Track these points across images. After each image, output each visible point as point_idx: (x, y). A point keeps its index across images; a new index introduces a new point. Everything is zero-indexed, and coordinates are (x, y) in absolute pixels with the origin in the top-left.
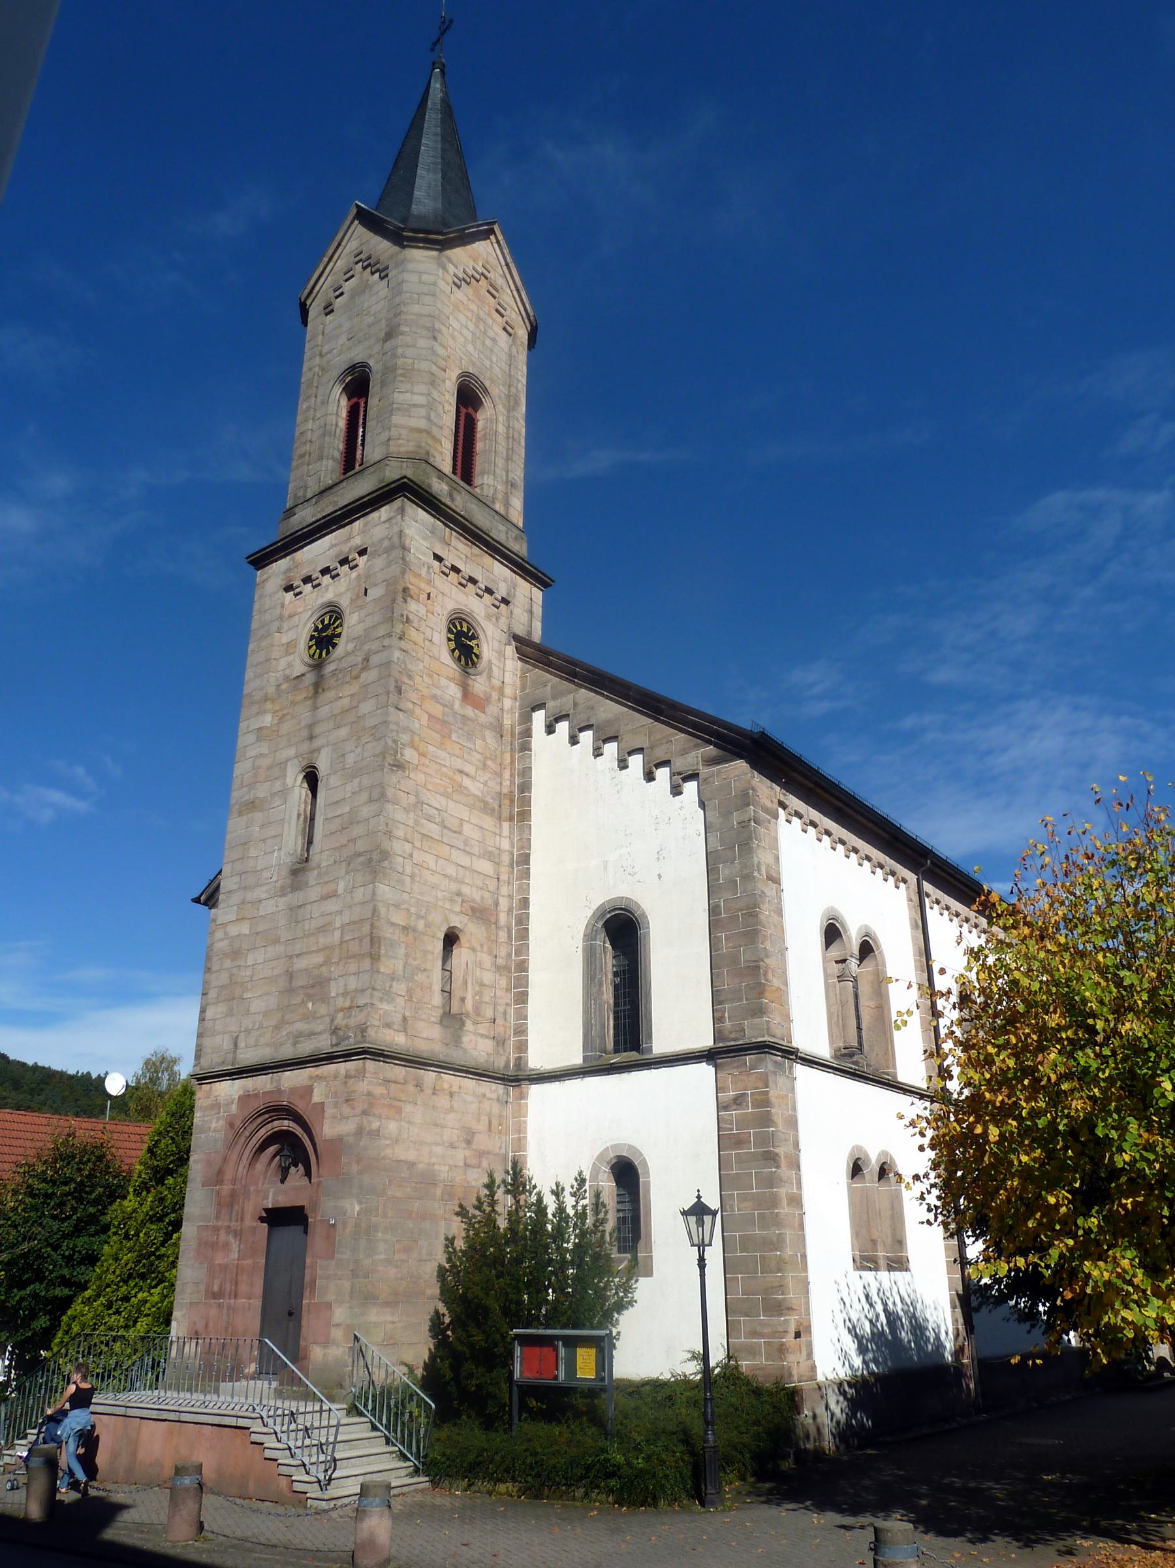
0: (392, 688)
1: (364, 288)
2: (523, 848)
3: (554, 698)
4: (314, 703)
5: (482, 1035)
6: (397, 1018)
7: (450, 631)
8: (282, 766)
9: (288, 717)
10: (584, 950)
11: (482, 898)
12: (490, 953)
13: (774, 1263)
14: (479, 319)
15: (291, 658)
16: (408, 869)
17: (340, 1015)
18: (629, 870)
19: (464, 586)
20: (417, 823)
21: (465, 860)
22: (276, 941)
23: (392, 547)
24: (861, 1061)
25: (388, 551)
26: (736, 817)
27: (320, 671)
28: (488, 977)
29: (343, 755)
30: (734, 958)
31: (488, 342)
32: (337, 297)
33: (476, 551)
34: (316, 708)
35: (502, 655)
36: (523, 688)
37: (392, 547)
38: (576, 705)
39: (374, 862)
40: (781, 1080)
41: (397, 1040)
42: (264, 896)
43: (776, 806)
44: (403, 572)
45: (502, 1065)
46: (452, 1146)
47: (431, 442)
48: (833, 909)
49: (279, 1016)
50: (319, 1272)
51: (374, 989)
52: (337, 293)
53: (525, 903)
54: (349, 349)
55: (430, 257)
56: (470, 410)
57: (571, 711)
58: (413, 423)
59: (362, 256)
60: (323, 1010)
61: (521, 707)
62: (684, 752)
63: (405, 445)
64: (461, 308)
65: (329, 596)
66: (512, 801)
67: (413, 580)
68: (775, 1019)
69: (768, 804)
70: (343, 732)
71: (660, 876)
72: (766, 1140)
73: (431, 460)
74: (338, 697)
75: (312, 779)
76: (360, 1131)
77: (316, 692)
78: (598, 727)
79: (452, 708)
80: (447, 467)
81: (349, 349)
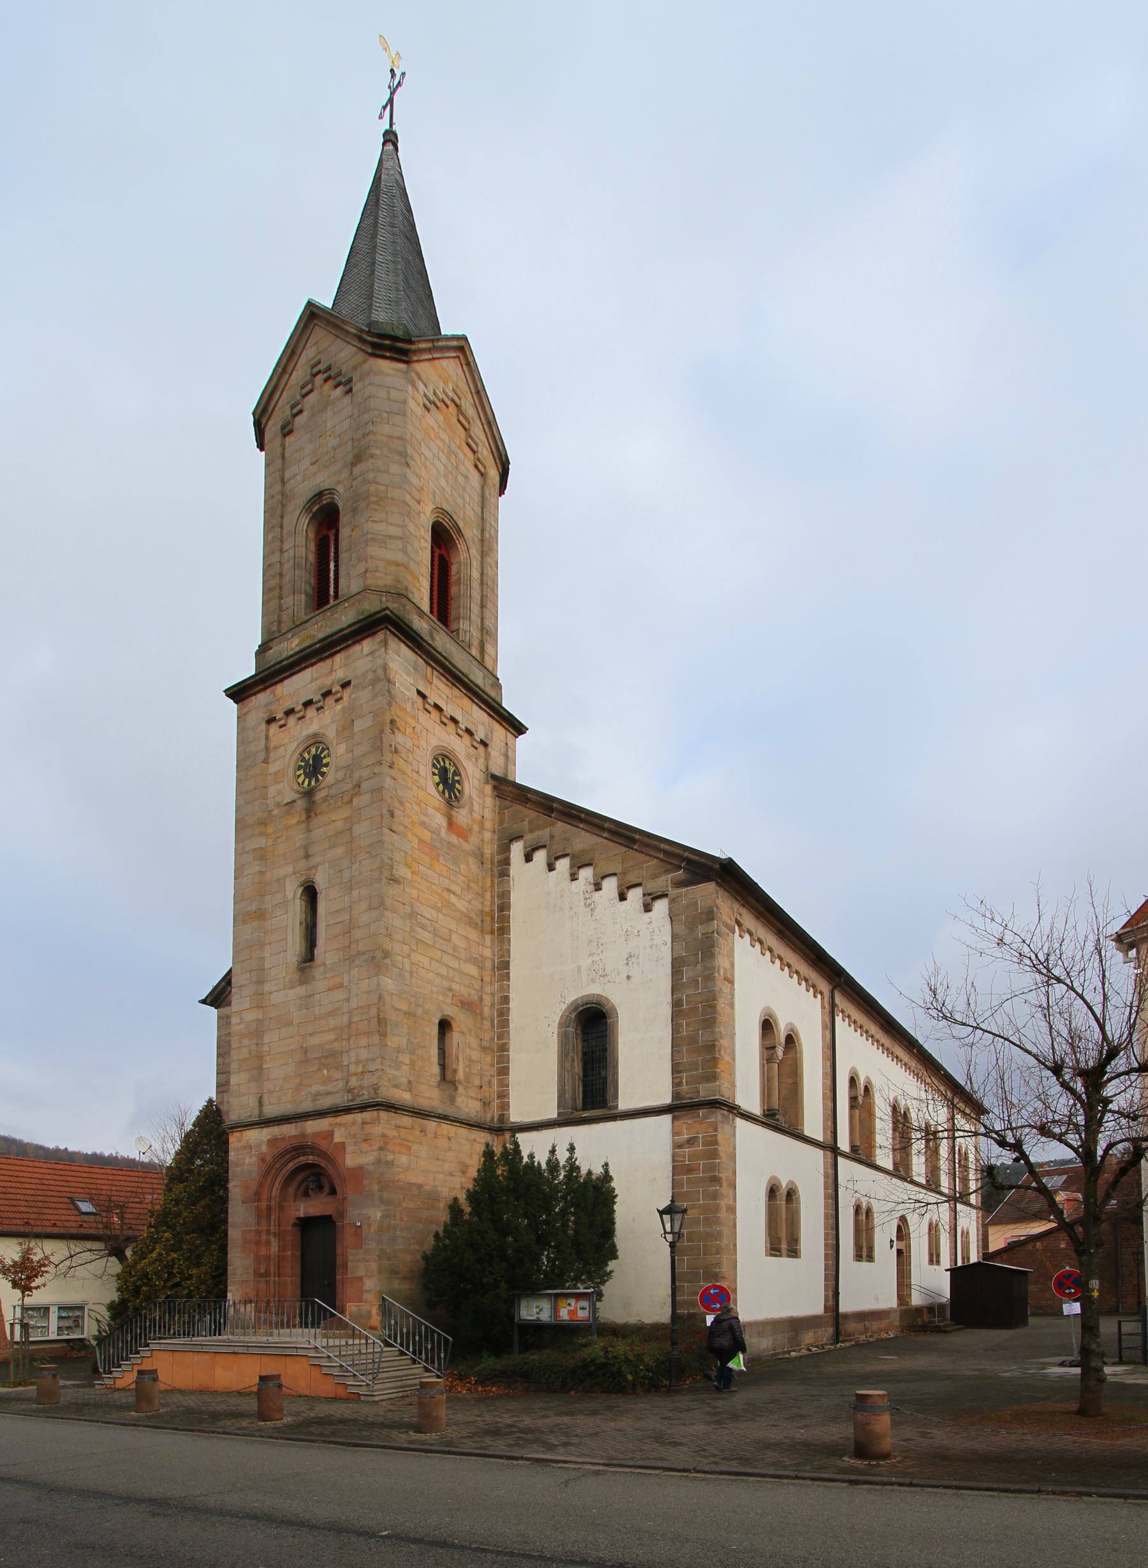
0: (385, 812)
1: (325, 405)
2: (502, 956)
3: (531, 831)
4: (308, 826)
5: (471, 1098)
6: (404, 1081)
7: (434, 766)
8: (281, 881)
9: (282, 839)
11: (469, 994)
12: (477, 1036)
13: (714, 1250)
14: (450, 451)
15: (280, 786)
16: (407, 967)
17: (354, 1079)
18: (601, 972)
19: (445, 724)
20: (412, 930)
21: (454, 964)
22: (291, 1024)
23: (377, 680)
24: (781, 1117)
25: (373, 683)
26: (701, 930)
27: (310, 798)
28: (475, 1055)
29: (341, 871)
30: (693, 1040)
31: (461, 479)
32: (295, 416)
33: (456, 692)
34: (309, 831)
35: (481, 792)
36: (501, 822)
37: (377, 680)
38: (552, 837)
39: (377, 960)
40: (727, 1128)
41: (406, 1097)
42: (273, 989)
43: (733, 923)
44: (390, 705)
45: (488, 1119)
46: (451, 1174)
47: (409, 578)
48: (768, 1008)
49: (297, 1080)
50: (350, 1258)
51: (383, 1058)
52: (295, 411)
53: (506, 1000)
54: (315, 474)
55: (398, 370)
56: (443, 552)
58: (390, 555)
59: (321, 367)
60: (338, 1075)
61: (500, 839)
62: (655, 876)
63: (383, 580)
64: (432, 435)
65: (314, 728)
66: (493, 918)
67: (399, 713)
68: (724, 1085)
69: (729, 921)
70: (340, 851)
72: (712, 1168)
73: (410, 596)
74: (331, 821)
75: (311, 894)
76: (378, 1161)
77: (308, 817)
79: (439, 835)
80: (426, 607)
81: (315, 474)
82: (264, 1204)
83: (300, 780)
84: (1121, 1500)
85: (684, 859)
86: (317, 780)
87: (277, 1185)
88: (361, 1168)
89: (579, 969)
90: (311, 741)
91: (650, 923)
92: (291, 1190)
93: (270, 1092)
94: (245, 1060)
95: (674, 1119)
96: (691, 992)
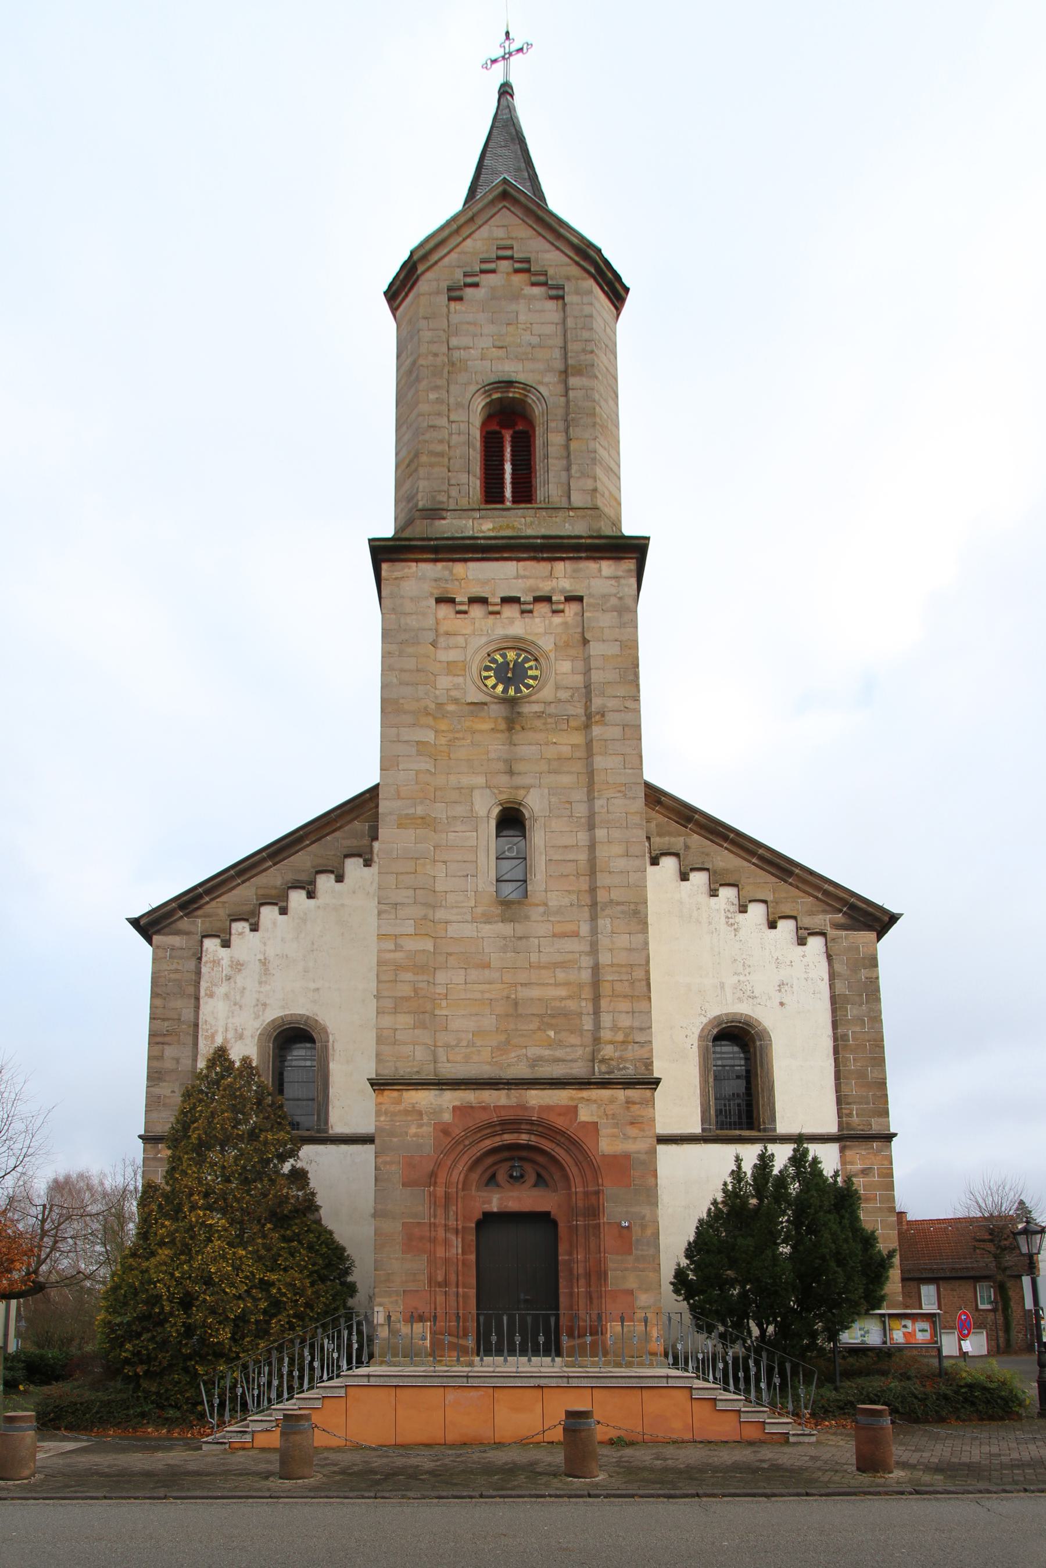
10: (699, 1047)
18: (749, 993)
22: (487, 966)
30: (861, 1075)
38: (687, 847)
42: (454, 918)
50: (611, 1265)
52: (469, 280)
57: (682, 852)
62: (811, 913)
71: (782, 1004)
75: (511, 820)
77: (510, 729)
78: (715, 872)
82: (440, 1191)
83: (491, 682)
84: (764, 1499)
85: (845, 902)
86: (518, 690)
87: (461, 1166)
88: (627, 1156)
89: (722, 986)
90: (509, 645)
91: (804, 956)
92: (475, 1176)
93: (447, 1046)
94: (407, 999)
95: (842, 1150)
96: (858, 1029)
